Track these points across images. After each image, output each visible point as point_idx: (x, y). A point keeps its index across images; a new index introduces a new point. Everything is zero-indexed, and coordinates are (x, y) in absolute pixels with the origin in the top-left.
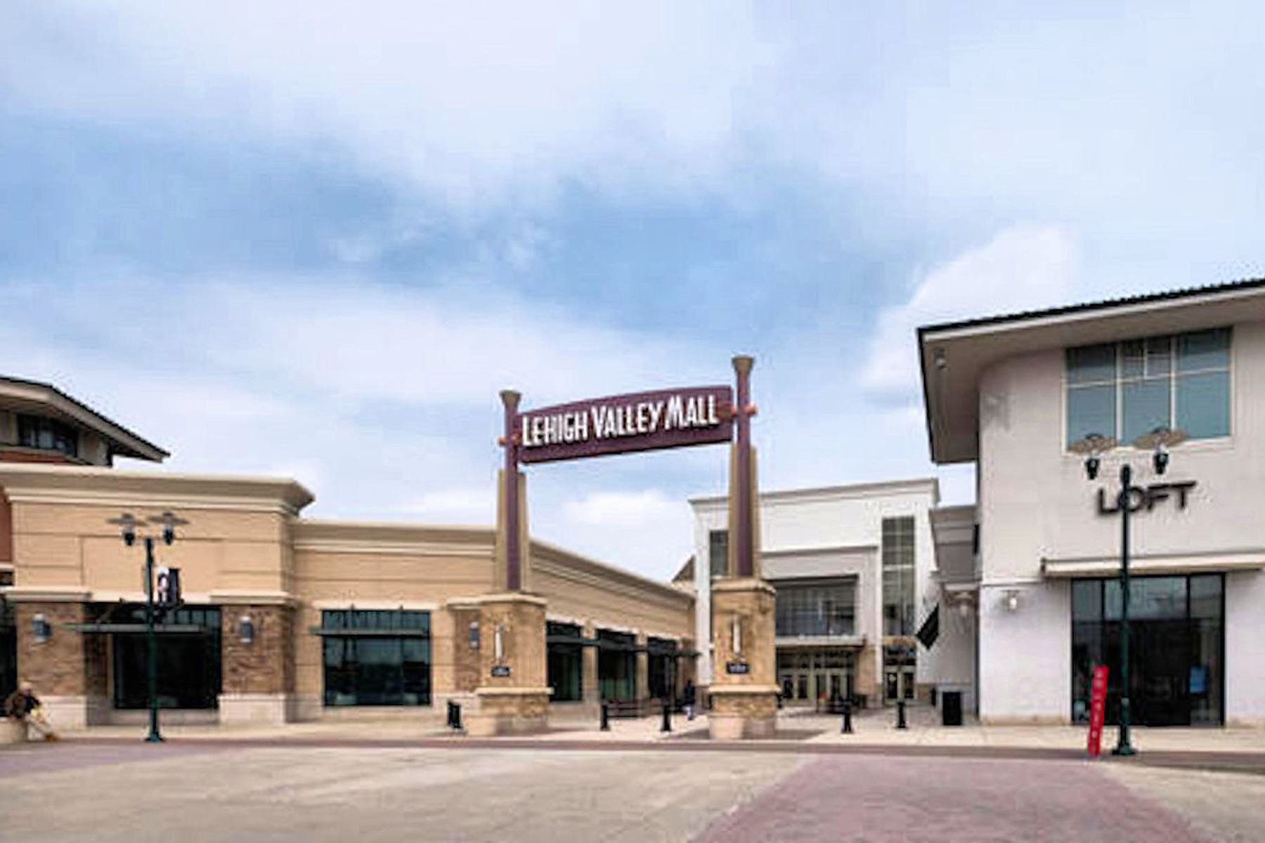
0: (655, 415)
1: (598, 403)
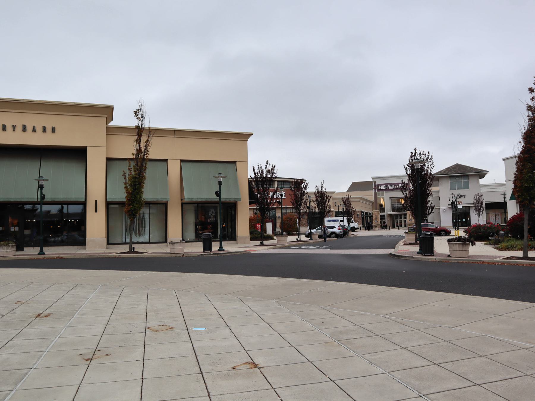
0: (397, 186)
1: (389, 184)
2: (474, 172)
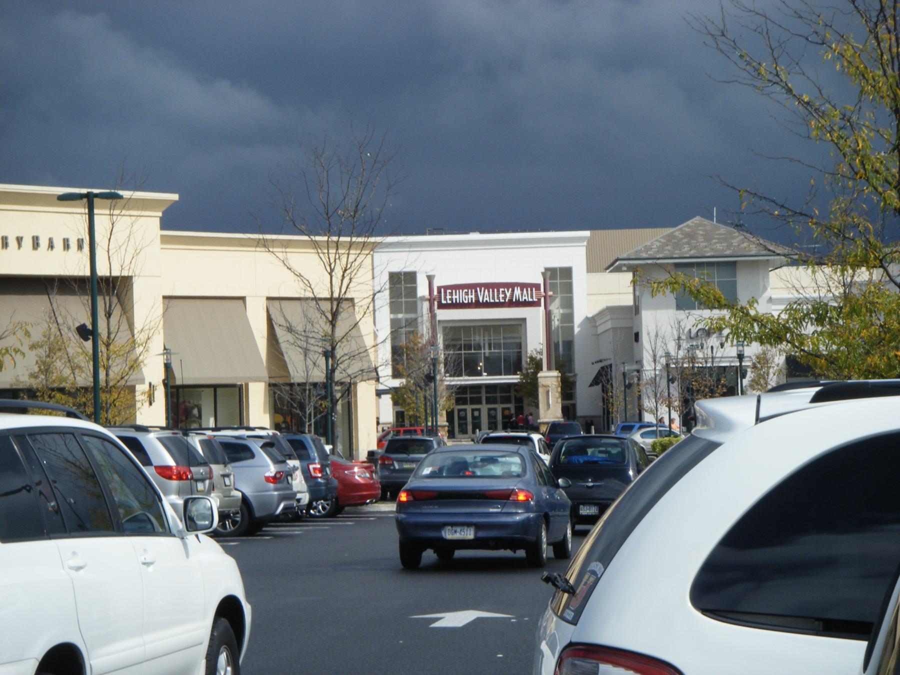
2: (753, 253)
